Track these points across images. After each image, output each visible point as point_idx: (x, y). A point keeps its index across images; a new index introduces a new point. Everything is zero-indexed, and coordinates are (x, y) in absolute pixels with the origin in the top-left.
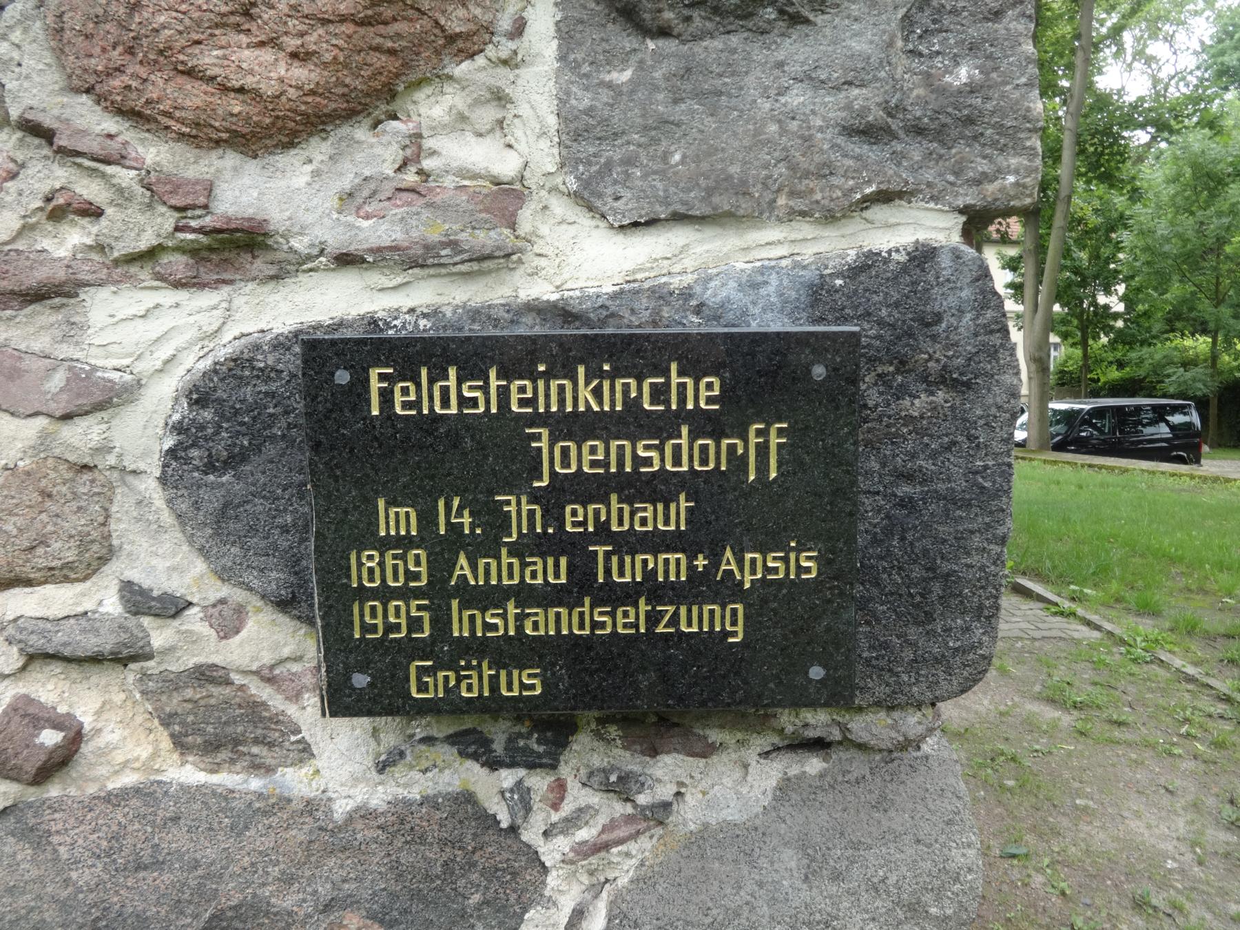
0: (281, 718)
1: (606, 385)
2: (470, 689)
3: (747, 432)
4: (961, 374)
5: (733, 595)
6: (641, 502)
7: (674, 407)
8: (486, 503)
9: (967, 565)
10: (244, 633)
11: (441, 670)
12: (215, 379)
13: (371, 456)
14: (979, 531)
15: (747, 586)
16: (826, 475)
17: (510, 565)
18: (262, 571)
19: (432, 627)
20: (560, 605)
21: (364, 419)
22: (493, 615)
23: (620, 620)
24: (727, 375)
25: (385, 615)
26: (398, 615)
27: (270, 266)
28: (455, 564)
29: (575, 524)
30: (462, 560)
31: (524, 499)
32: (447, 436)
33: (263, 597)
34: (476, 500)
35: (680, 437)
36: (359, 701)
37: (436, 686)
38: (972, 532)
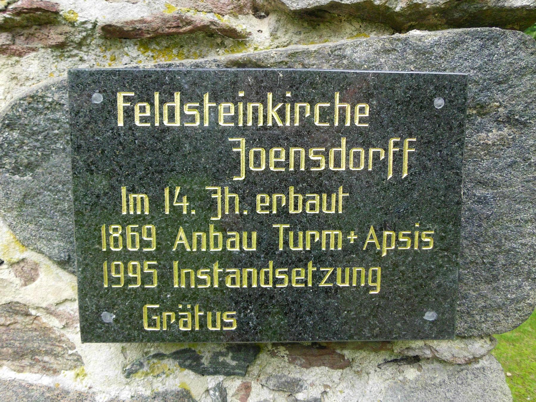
0: (63, 338)
1: (288, 107)
2: (185, 325)
3: (387, 143)
4: (521, 116)
5: (374, 260)
6: (311, 193)
7: (336, 124)
8: (200, 192)
9: (521, 244)
10: (37, 282)
11: (165, 311)
12: (20, 110)
13: (117, 156)
14: (531, 221)
15: (384, 254)
16: (442, 176)
17: (216, 237)
18: (49, 240)
19: (159, 281)
20: (251, 266)
21: (112, 129)
22: (202, 273)
23: (294, 278)
24: (375, 102)
25: (126, 272)
26: (135, 272)
27: (60, 36)
28: (176, 236)
29: (263, 208)
30: (181, 233)
31: (227, 189)
32: (172, 143)
33: (50, 258)
34: (191, 189)
35: (340, 146)
36: (107, 331)
37: (161, 322)
38: (526, 222)
